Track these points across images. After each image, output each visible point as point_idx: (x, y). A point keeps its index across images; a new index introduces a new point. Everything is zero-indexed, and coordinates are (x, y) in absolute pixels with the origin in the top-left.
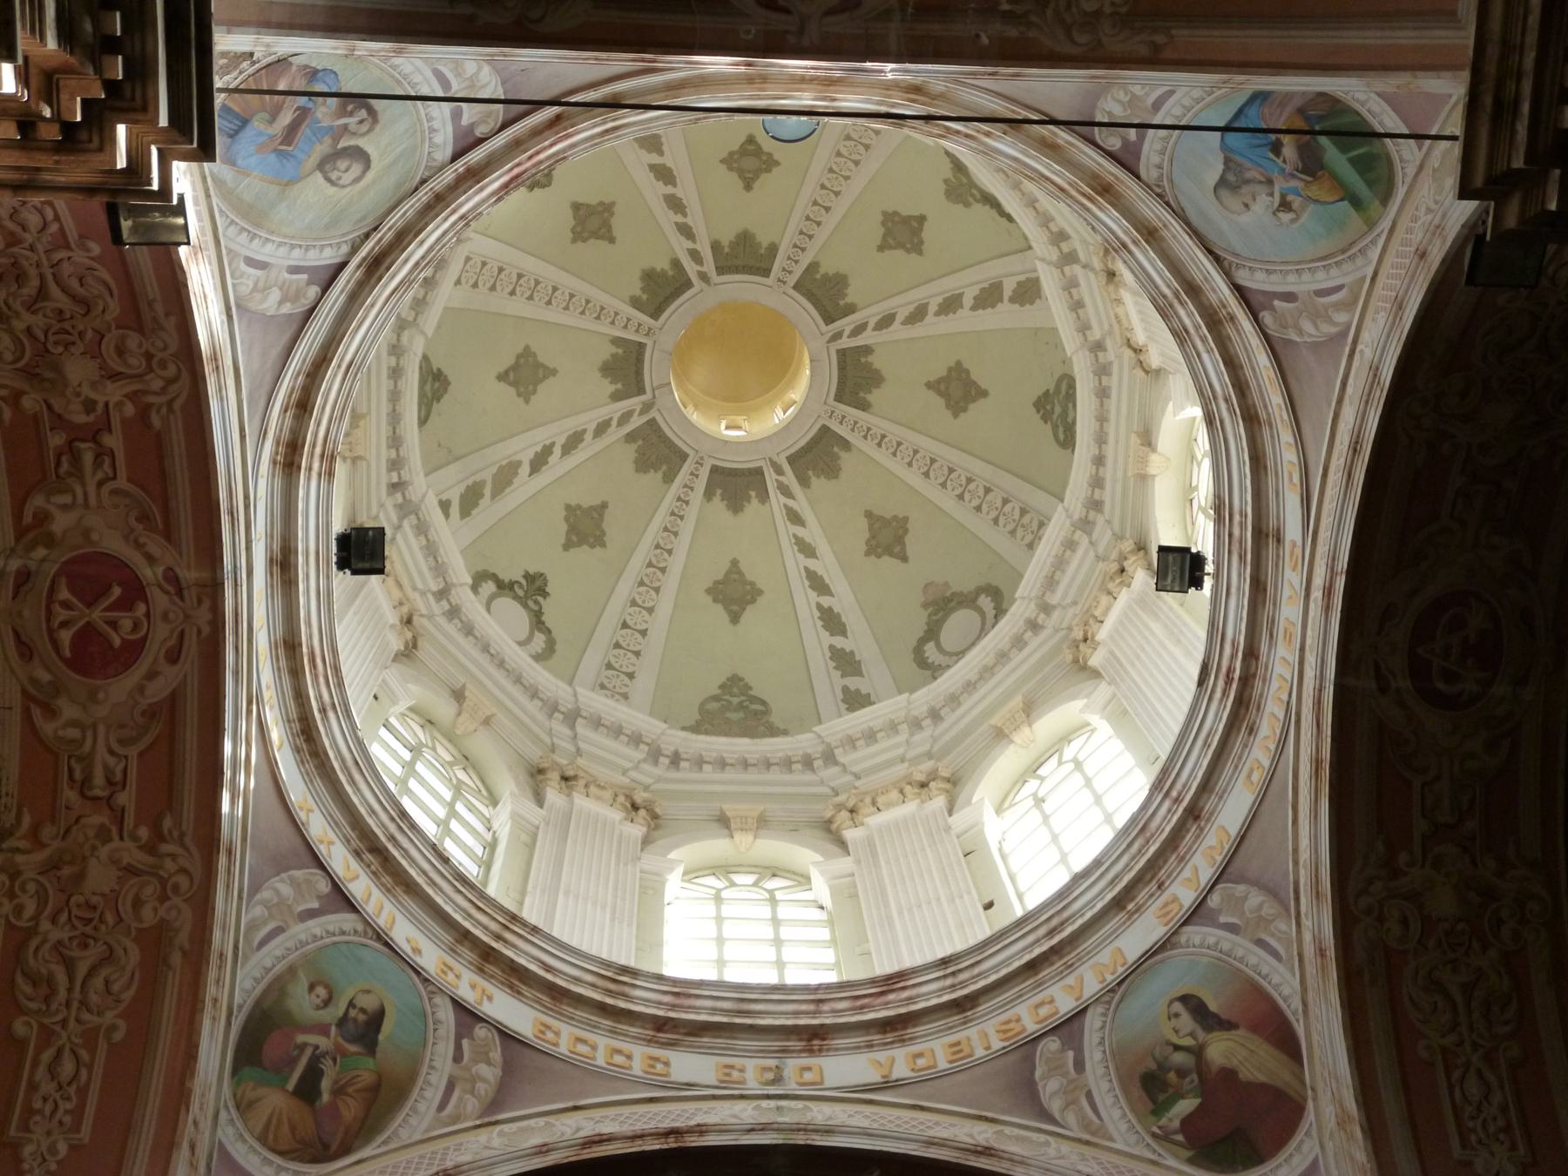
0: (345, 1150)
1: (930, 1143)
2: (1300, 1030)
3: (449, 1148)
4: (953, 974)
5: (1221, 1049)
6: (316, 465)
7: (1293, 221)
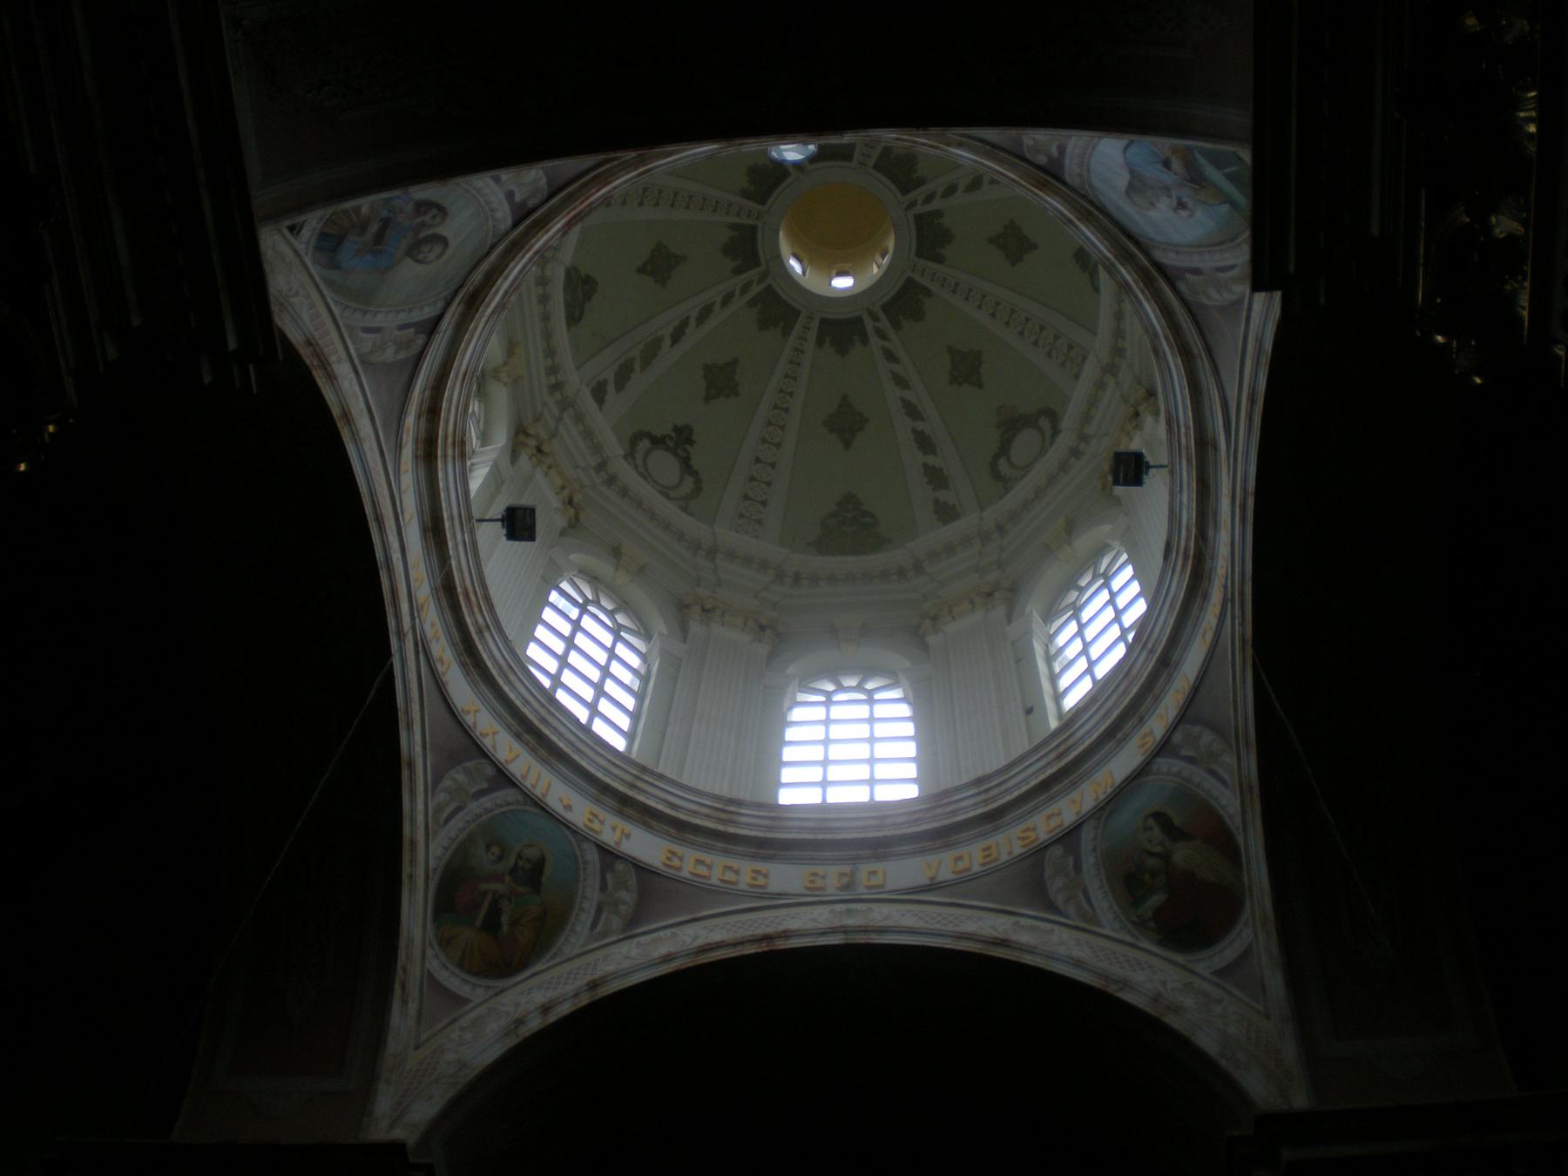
0: (523, 965)
1: (961, 937)
2: (1241, 840)
3: (599, 959)
4: (987, 791)
5: (1182, 855)
6: (450, 452)
7: (1191, 216)
